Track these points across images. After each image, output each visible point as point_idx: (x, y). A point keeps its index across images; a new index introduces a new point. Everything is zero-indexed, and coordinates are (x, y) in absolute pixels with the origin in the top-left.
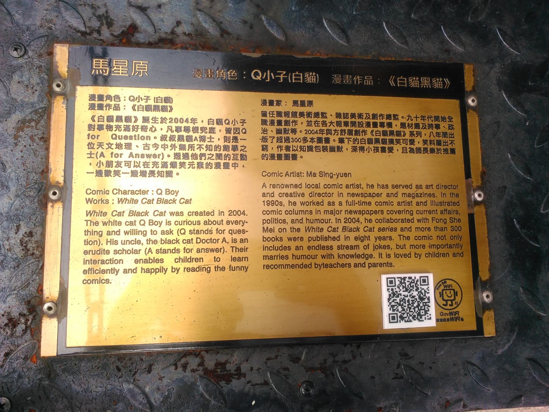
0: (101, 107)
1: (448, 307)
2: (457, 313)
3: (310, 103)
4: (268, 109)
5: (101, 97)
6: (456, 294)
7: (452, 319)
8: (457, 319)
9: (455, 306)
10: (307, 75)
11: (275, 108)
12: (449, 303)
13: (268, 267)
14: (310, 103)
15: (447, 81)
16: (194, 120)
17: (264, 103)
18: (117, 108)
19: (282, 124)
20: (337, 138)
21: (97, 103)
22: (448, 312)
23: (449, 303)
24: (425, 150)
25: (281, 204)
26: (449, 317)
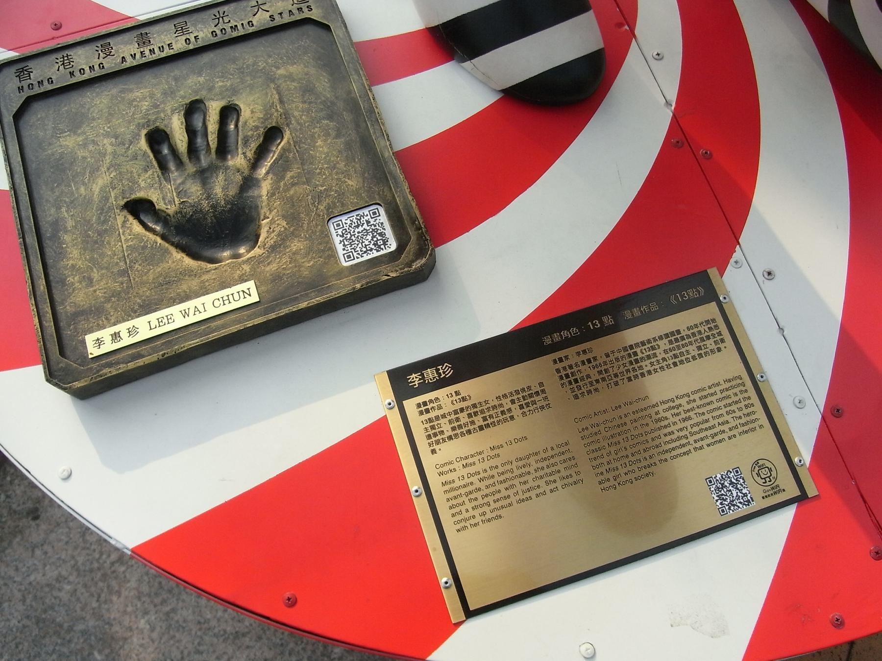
0: (427, 411)
1: (768, 483)
2: (778, 486)
3: (566, 357)
4: (560, 365)
5: (425, 404)
6: (770, 470)
7: (775, 493)
8: (779, 491)
9: (773, 481)
10: (605, 319)
11: (565, 363)
12: (768, 479)
13: (458, 531)
14: (566, 357)
15: (700, 289)
16: (529, 388)
17: (555, 362)
18: (440, 407)
19: (569, 379)
20: (694, 347)
21: (423, 408)
22: (769, 488)
23: (768, 479)
24: (456, 435)
25: (666, 418)
26: (771, 492)
